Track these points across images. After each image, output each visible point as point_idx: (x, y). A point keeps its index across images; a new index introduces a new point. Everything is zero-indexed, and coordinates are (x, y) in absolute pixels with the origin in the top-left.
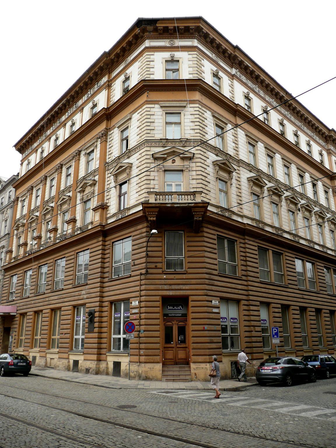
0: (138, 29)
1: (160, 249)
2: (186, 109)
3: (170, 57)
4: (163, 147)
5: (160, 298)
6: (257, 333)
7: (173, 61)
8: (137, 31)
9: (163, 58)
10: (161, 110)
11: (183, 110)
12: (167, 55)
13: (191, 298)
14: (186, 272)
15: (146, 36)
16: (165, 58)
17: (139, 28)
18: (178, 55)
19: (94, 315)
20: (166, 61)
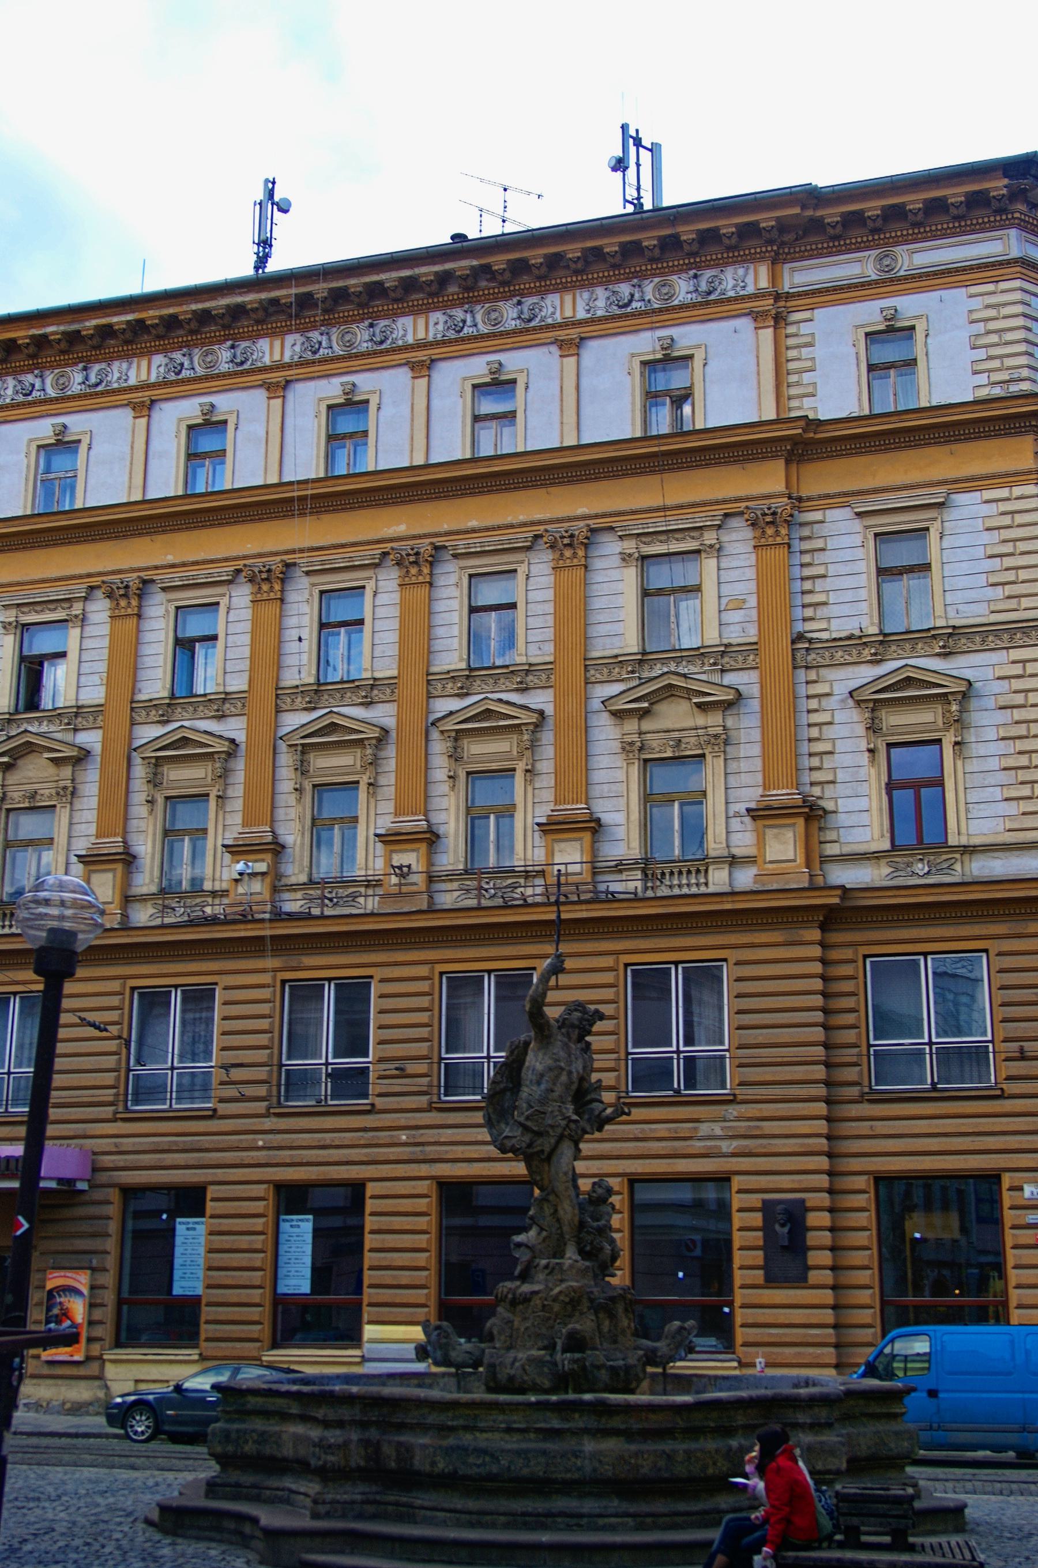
0: (1006, 181)
1: (424, 1032)
2: (950, 514)
3: (880, 318)
4: (457, 695)
5: (267, 1190)
6: (214, 1309)
7: (499, 384)
8: (998, 186)
9: (857, 327)
10: (857, 525)
11: (935, 519)
12: (869, 312)
13: (212, 1192)
14: (998, 1092)
15: (1017, 215)
16: (862, 326)
17: (1010, 178)
18: (909, 305)
19: (804, 1219)
20: (475, 387)
